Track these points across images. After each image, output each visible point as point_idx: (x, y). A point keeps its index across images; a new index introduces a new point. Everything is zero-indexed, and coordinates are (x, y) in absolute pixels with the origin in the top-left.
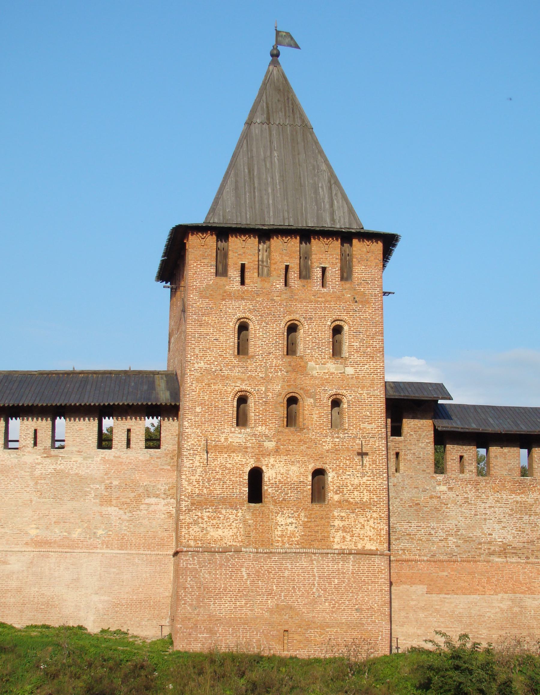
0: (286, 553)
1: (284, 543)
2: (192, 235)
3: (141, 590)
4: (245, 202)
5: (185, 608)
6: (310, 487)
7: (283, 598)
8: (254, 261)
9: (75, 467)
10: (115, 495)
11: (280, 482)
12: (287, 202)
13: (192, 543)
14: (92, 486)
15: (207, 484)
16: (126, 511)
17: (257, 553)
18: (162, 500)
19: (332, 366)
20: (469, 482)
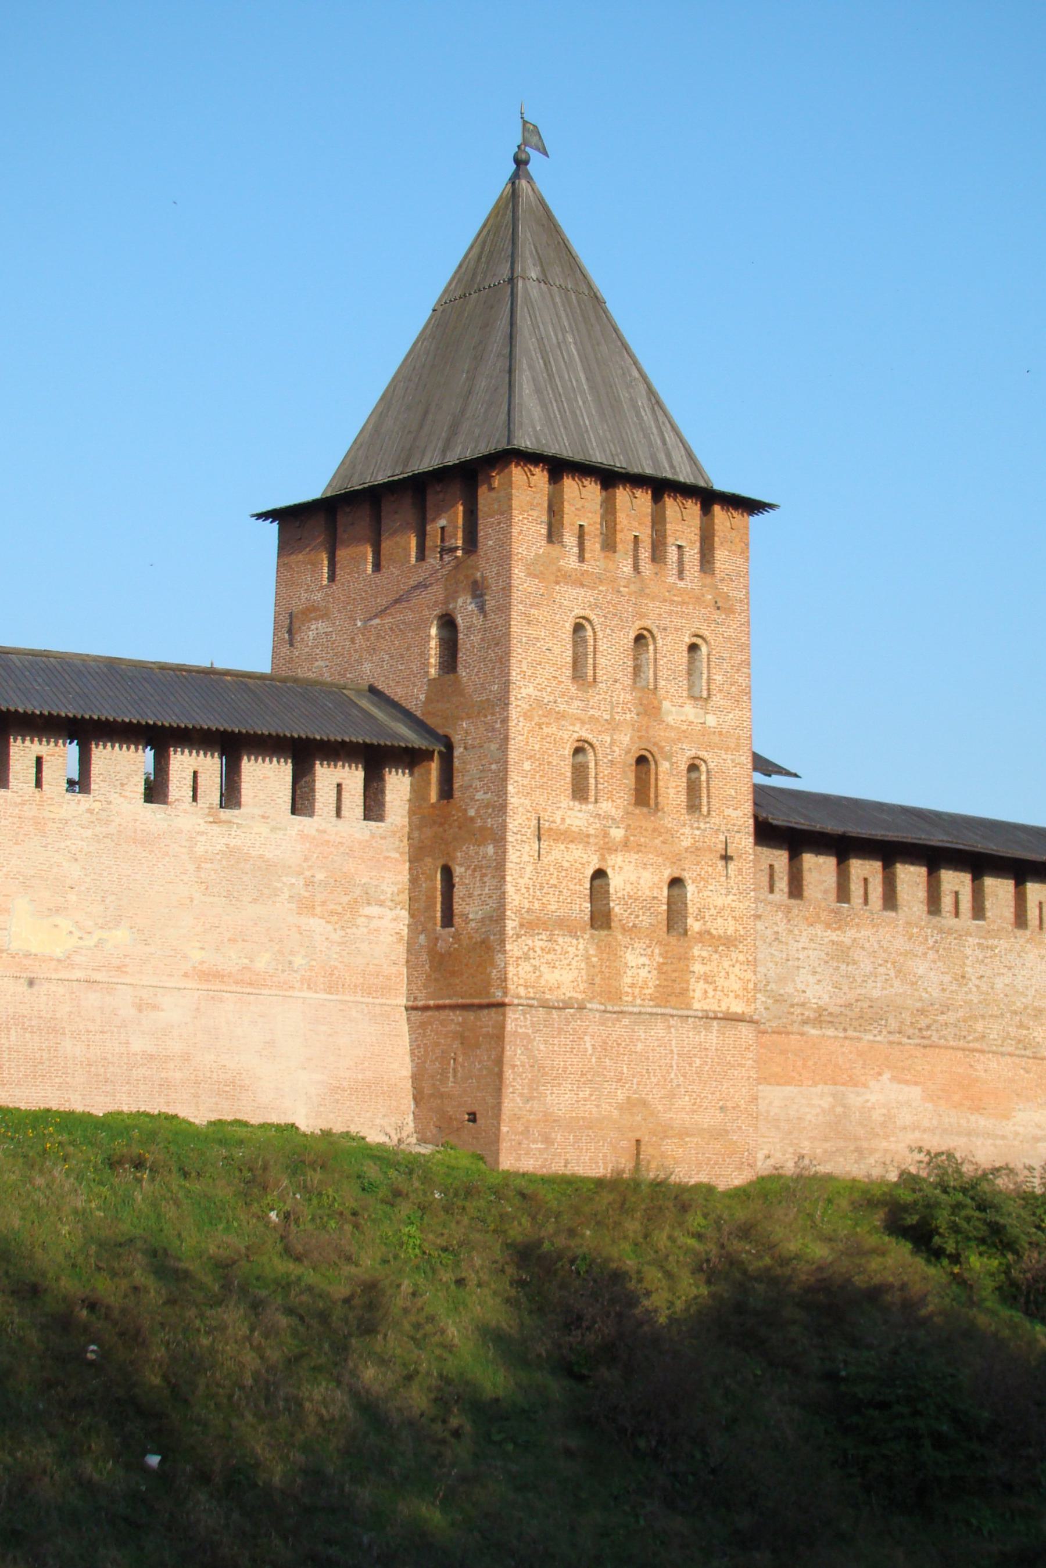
0: (640, 1013)
1: (634, 997)
2: (517, 465)
3: (366, 1064)
4: (555, 417)
5: (513, 1100)
6: (665, 907)
7: (635, 1087)
8: (595, 523)
9: (258, 844)
10: (319, 898)
11: (630, 897)
12: (608, 426)
13: (522, 991)
14: (284, 879)
15: (538, 893)
16: (337, 926)
17: (605, 1011)
18: (389, 911)
19: (690, 711)
20: (779, 907)
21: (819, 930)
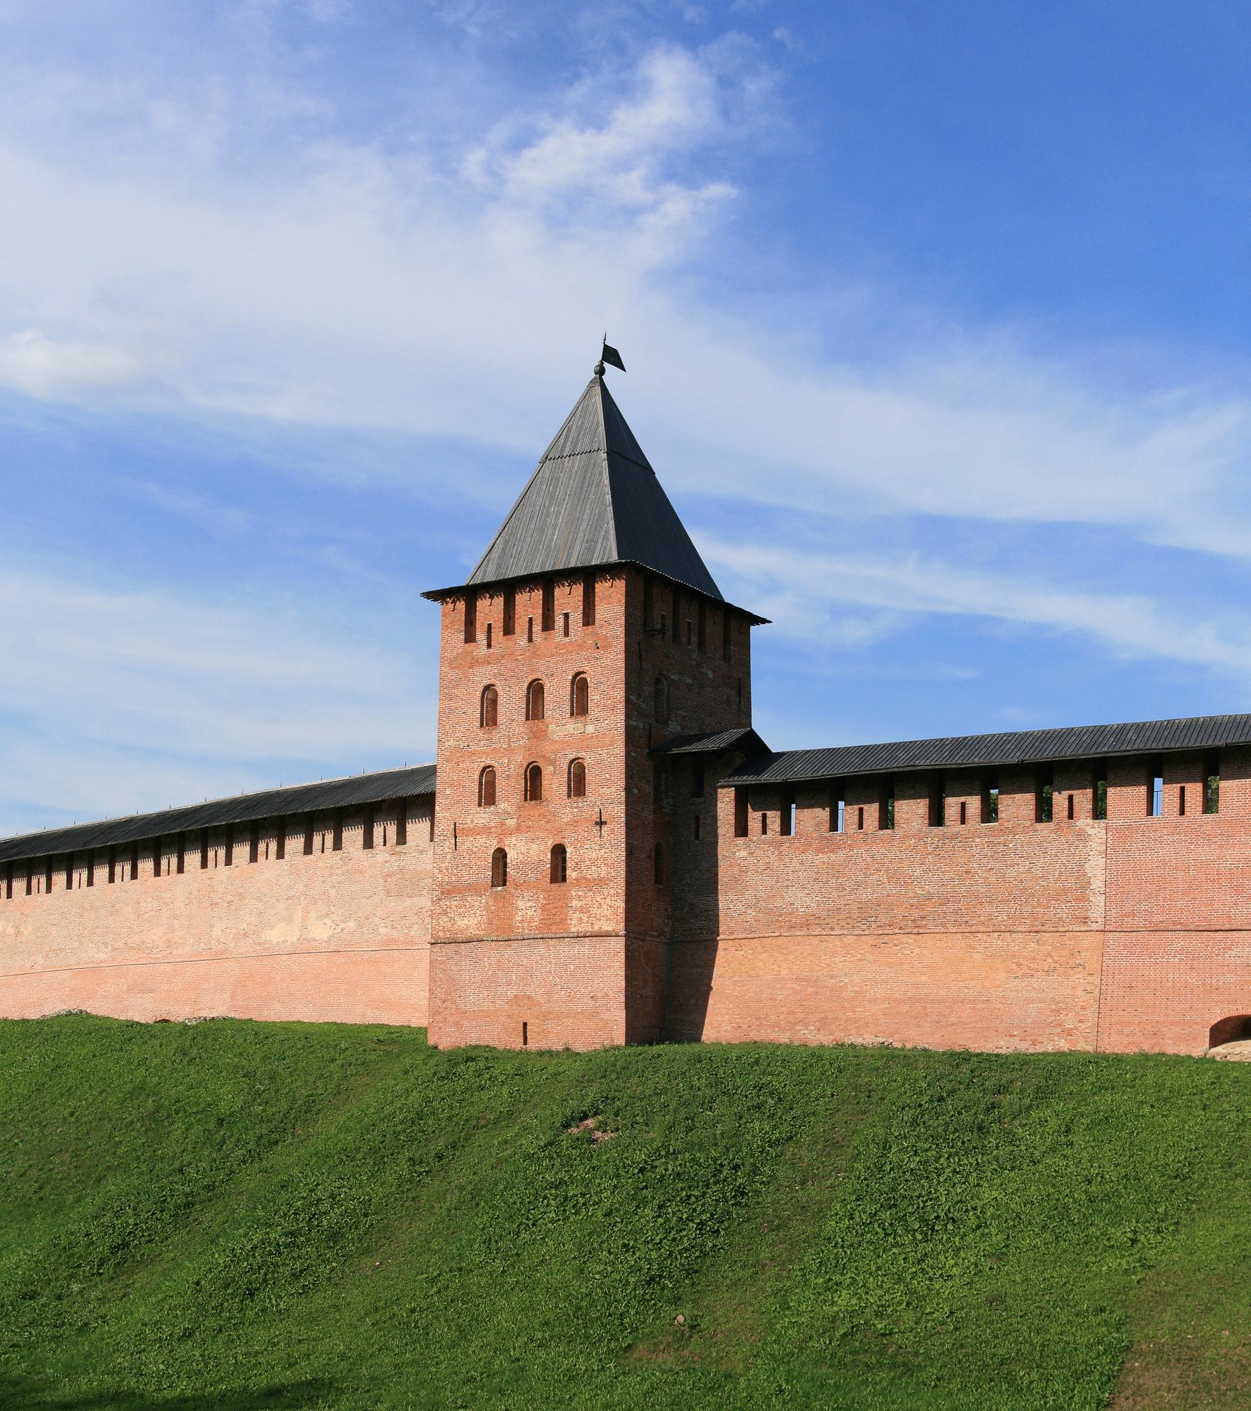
21: (810, 856)
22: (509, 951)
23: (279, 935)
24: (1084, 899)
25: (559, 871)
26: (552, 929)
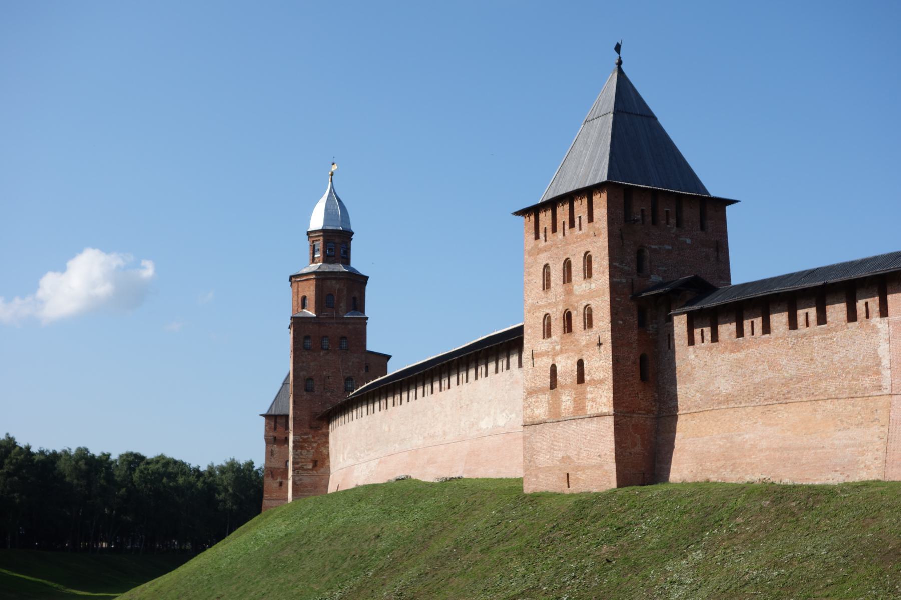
21: (727, 355)
22: (560, 428)
23: (485, 424)
24: (878, 373)
25: (581, 379)
26: (579, 414)
